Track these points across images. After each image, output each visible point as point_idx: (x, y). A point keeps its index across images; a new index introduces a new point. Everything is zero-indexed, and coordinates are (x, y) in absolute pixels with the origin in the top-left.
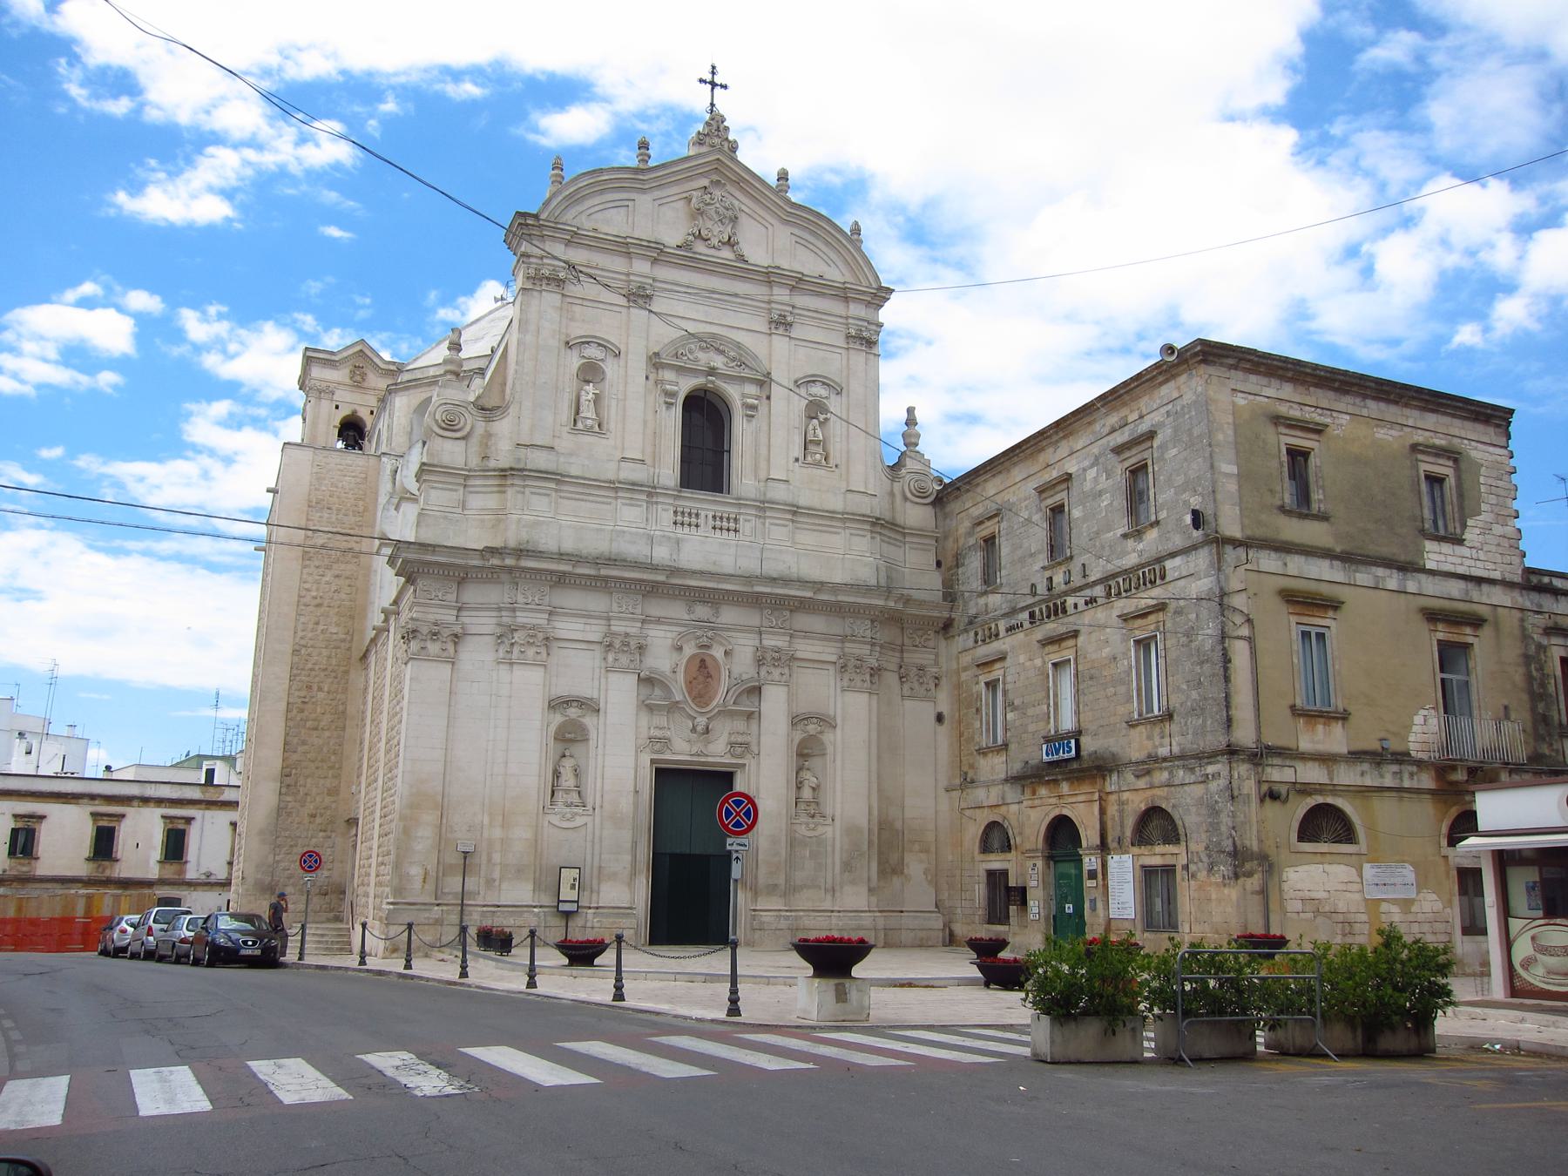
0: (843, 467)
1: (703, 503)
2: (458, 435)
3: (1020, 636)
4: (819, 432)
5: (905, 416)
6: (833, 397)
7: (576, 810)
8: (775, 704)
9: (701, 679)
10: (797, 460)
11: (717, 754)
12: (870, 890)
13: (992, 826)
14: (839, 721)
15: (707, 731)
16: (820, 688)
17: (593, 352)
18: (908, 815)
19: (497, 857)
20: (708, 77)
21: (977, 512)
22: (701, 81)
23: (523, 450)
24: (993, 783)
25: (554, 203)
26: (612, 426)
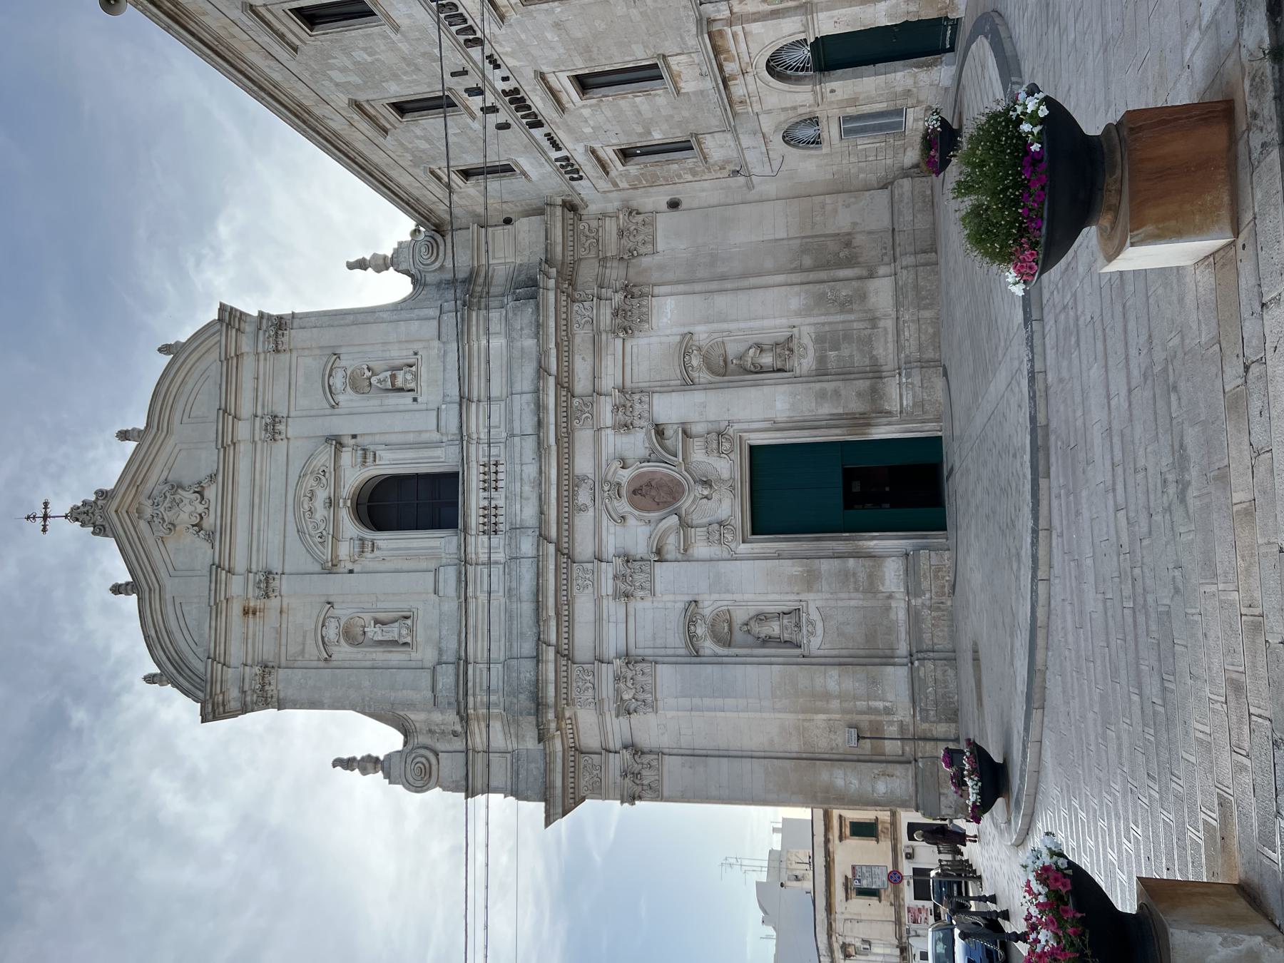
0: (416, 346)
1: (474, 500)
2: (433, 760)
3: (561, 135)
4: (381, 376)
5: (358, 271)
7: (804, 620)
8: (669, 409)
9: (654, 493)
10: (415, 400)
11: (729, 468)
13: (788, 139)
14: (686, 330)
15: (707, 483)
16: (649, 351)
17: (332, 632)
18: (782, 234)
19: (861, 704)
20: (39, 522)
21: (434, 187)
22: (44, 530)
23: (439, 699)
25: (186, 684)
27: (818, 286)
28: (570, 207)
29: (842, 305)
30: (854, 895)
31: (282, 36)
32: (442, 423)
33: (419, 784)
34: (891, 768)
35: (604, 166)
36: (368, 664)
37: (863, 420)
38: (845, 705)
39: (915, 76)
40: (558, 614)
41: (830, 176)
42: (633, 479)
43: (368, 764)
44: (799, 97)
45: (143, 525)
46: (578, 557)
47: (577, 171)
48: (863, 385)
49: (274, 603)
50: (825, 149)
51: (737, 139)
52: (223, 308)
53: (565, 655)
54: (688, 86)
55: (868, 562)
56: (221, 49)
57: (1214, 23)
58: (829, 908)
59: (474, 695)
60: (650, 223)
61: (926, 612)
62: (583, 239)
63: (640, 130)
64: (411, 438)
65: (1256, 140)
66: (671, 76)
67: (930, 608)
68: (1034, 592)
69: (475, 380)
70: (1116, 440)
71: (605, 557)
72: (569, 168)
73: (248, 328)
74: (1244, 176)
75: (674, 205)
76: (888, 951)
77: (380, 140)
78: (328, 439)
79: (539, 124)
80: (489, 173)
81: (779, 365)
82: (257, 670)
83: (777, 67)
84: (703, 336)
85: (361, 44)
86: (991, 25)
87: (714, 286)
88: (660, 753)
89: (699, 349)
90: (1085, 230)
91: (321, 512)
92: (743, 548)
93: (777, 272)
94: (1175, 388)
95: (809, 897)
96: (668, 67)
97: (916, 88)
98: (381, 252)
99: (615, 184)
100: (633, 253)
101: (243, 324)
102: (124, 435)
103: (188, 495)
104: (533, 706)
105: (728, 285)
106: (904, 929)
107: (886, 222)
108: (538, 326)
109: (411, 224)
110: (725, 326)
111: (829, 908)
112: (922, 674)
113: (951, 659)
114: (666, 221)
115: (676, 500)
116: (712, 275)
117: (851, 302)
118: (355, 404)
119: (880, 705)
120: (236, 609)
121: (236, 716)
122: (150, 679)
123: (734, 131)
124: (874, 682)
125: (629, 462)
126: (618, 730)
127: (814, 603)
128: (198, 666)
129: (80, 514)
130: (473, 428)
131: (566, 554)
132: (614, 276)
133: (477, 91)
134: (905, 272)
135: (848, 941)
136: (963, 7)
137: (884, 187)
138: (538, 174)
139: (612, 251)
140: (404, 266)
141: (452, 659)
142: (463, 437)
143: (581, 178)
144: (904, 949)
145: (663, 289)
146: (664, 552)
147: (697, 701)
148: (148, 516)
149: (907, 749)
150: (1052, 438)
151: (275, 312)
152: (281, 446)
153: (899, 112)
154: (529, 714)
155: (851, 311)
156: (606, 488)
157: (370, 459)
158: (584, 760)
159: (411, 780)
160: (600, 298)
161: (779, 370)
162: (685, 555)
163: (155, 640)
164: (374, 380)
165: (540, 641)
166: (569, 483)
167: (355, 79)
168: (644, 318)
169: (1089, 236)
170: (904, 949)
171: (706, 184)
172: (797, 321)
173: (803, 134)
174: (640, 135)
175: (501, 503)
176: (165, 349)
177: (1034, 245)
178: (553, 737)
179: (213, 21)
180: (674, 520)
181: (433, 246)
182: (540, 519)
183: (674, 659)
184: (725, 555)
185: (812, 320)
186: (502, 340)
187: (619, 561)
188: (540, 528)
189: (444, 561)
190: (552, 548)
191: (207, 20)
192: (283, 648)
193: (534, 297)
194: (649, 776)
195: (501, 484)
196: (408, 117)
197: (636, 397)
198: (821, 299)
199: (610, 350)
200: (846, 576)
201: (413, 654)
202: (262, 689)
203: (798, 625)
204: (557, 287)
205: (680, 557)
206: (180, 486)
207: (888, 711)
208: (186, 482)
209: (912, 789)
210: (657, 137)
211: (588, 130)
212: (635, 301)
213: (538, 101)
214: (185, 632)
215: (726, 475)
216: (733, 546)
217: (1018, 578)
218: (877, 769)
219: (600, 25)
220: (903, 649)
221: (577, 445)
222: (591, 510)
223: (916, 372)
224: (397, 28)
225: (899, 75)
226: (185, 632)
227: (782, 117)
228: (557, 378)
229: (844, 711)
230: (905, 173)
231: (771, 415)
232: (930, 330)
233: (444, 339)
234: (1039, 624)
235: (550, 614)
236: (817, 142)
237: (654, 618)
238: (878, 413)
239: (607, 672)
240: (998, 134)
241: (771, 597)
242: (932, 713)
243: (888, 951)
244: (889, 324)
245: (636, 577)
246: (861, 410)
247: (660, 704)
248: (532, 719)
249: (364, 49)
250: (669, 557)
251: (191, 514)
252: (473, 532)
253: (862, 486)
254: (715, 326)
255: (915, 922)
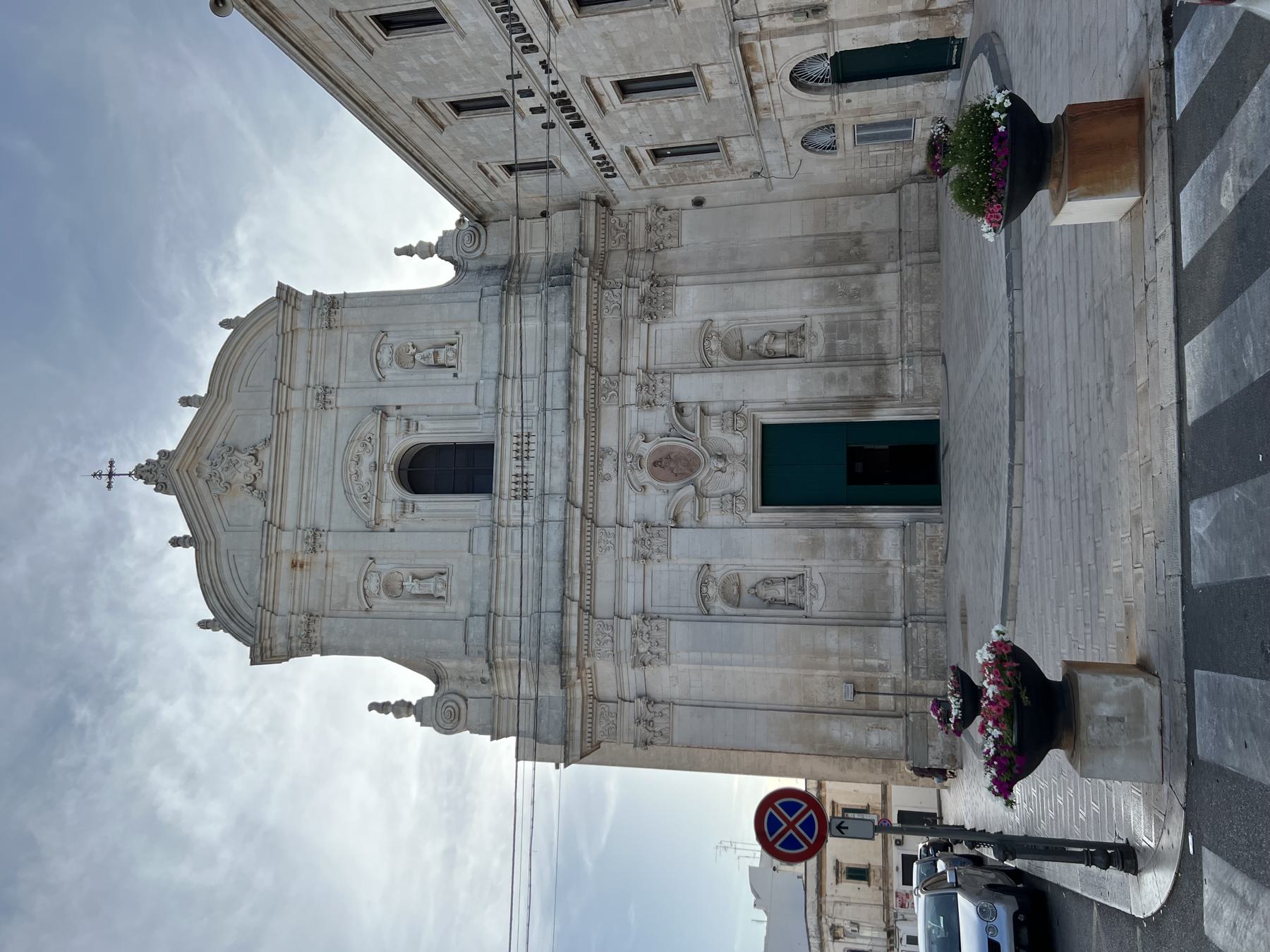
0: (458, 327)
1: (505, 469)
2: (463, 705)
3: (600, 136)
4: (425, 353)
5: (404, 257)
6: (391, 339)
7: (807, 584)
8: (689, 388)
9: (672, 465)
10: (455, 375)
11: (744, 444)
12: (879, 273)
13: (806, 144)
14: (706, 317)
15: (722, 457)
17: (373, 586)
18: (797, 232)
19: (858, 662)
21: (482, 181)
22: (109, 487)
23: (470, 648)
24: (762, 152)
26: (440, 562)
27: (829, 280)
28: (603, 202)
29: (851, 297)
30: (844, 878)
31: (361, 40)
32: (480, 397)
33: (449, 726)
34: (884, 720)
35: (637, 165)
36: (406, 615)
37: (867, 403)
38: (843, 662)
39: (923, 89)
40: (581, 573)
41: (843, 180)
42: (654, 452)
43: (401, 709)
44: (819, 105)
45: (201, 483)
46: (601, 521)
47: (612, 169)
48: (869, 370)
49: (321, 557)
50: (839, 155)
51: (760, 143)
52: (280, 287)
53: (587, 610)
54: (718, 93)
55: (868, 533)
56: (307, 50)
57: (1135, 43)
58: (820, 890)
59: (503, 645)
60: (676, 219)
61: (920, 579)
62: (614, 232)
63: (671, 132)
64: (450, 410)
65: (1155, 125)
66: (704, 84)
67: (924, 575)
68: (1009, 519)
69: (511, 359)
70: (1070, 371)
71: (625, 522)
72: (605, 166)
73: (302, 306)
74: (1148, 153)
75: (698, 203)
76: (876, 934)
77: (437, 135)
78: (375, 409)
79: (579, 124)
80: (522, 169)
81: (791, 351)
82: (303, 618)
83: (799, 78)
84: (722, 323)
85: (430, 48)
86: (990, 44)
87: (734, 277)
88: (672, 703)
89: (718, 335)
90: (1039, 193)
91: (366, 475)
92: (754, 517)
93: (792, 266)
94: (1107, 317)
95: (800, 882)
96: (702, 76)
97: (929, 101)
98: (426, 240)
99: (646, 183)
100: (660, 246)
101: (298, 303)
102: (186, 402)
103: (244, 457)
104: (557, 655)
105: (747, 276)
106: (892, 913)
107: (893, 224)
108: (571, 309)
109: (456, 214)
110: (743, 314)
111: (820, 890)
112: (914, 634)
113: (942, 621)
114: (690, 217)
115: (693, 472)
116: (731, 268)
117: (859, 295)
118: (400, 378)
119: (875, 662)
120: (285, 562)
121: (280, 662)
122: (204, 625)
123: (757, 135)
124: (870, 641)
125: (649, 436)
126: (633, 679)
127: (817, 569)
128: (248, 613)
129: (145, 472)
130: (508, 403)
131: (590, 519)
132: (641, 266)
133: (528, 93)
134: (909, 268)
135: (837, 922)
136: (968, 28)
137: (893, 191)
138: (576, 170)
139: (640, 243)
140: (448, 253)
141: (484, 612)
142: (499, 409)
143: (615, 176)
144: (891, 933)
145: (686, 279)
146: (680, 519)
147: (707, 655)
148: (206, 476)
149: (899, 704)
150: (1027, 386)
151: (328, 291)
152: (331, 414)
153: (908, 122)
154: (553, 663)
155: (859, 303)
156: (629, 460)
157: (413, 428)
158: (601, 707)
159: (441, 722)
160: (628, 286)
161: (791, 356)
162: (700, 522)
163: (210, 589)
164: (417, 356)
165: (564, 597)
166: (595, 455)
167: (420, 79)
168: (669, 305)
169: (1043, 197)
170: (891, 933)
171: (729, 184)
172: (809, 311)
173: (818, 140)
174: (672, 137)
175: (532, 471)
176: (225, 324)
177: (1000, 200)
178: (574, 685)
179: (302, 25)
180: (690, 490)
181: (475, 235)
182: (568, 486)
183: (687, 617)
184: (737, 523)
185: (823, 310)
186: (537, 322)
187: (639, 527)
188: (568, 494)
189: (478, 523)
190: (578, 512)
191: (296, 23)
192: (327, 599)
193: (568, 284)
194: (660, 724)
195: (532, 454)
196: (464, 115)
197: (659, 377)
198: (831, 292)
199: (637, 331)
200: (848, 545)
201: (447, 607)
202: (307, 636)
203: (802, 589)
204: (589, 275)
205: (694, 524)
206: (236, 449)
207: (882, 668)
208: (242, 447)
209: (902, 741)
210: (687, 139)
211: (625, 131)
212: (660, 290)
213: (582, 104)
214: (237, 582)
215: (739, 450)
216: (744, 515)
217: (997, 515)
218: (871, 722)
219: (644, 37)
220: (898, 612)
221: (604, 420)
222: (614, 479)
223: (917, 360)
224: (463, 35)
225: (910, 87)
226: (237, 582)
227: (802, 123)
228: (586, 358)
229: (842, 668)
230: (913, 178)
231: (782, 396)
232: (931, 323)
233: (483, 320)
234: (1013, 545)
235: (575, 570)
236: (832, 147)
237: (670, 579)
238: (881, 396)
239: (625, 627)
240: (976, 122)
241: (777, 563)
242: (923, 671)
243: (876, 934)
244: (893, 316)
245: (654, 541)
246: (867, 393)
247: (673, 657)
248: (555, 668)
249: (432, 53)
250: (684, 524)
251: (246, 475)
252: (506, 497)
253: (865, 465)
254: (733, 314)
255: (903, 906)
